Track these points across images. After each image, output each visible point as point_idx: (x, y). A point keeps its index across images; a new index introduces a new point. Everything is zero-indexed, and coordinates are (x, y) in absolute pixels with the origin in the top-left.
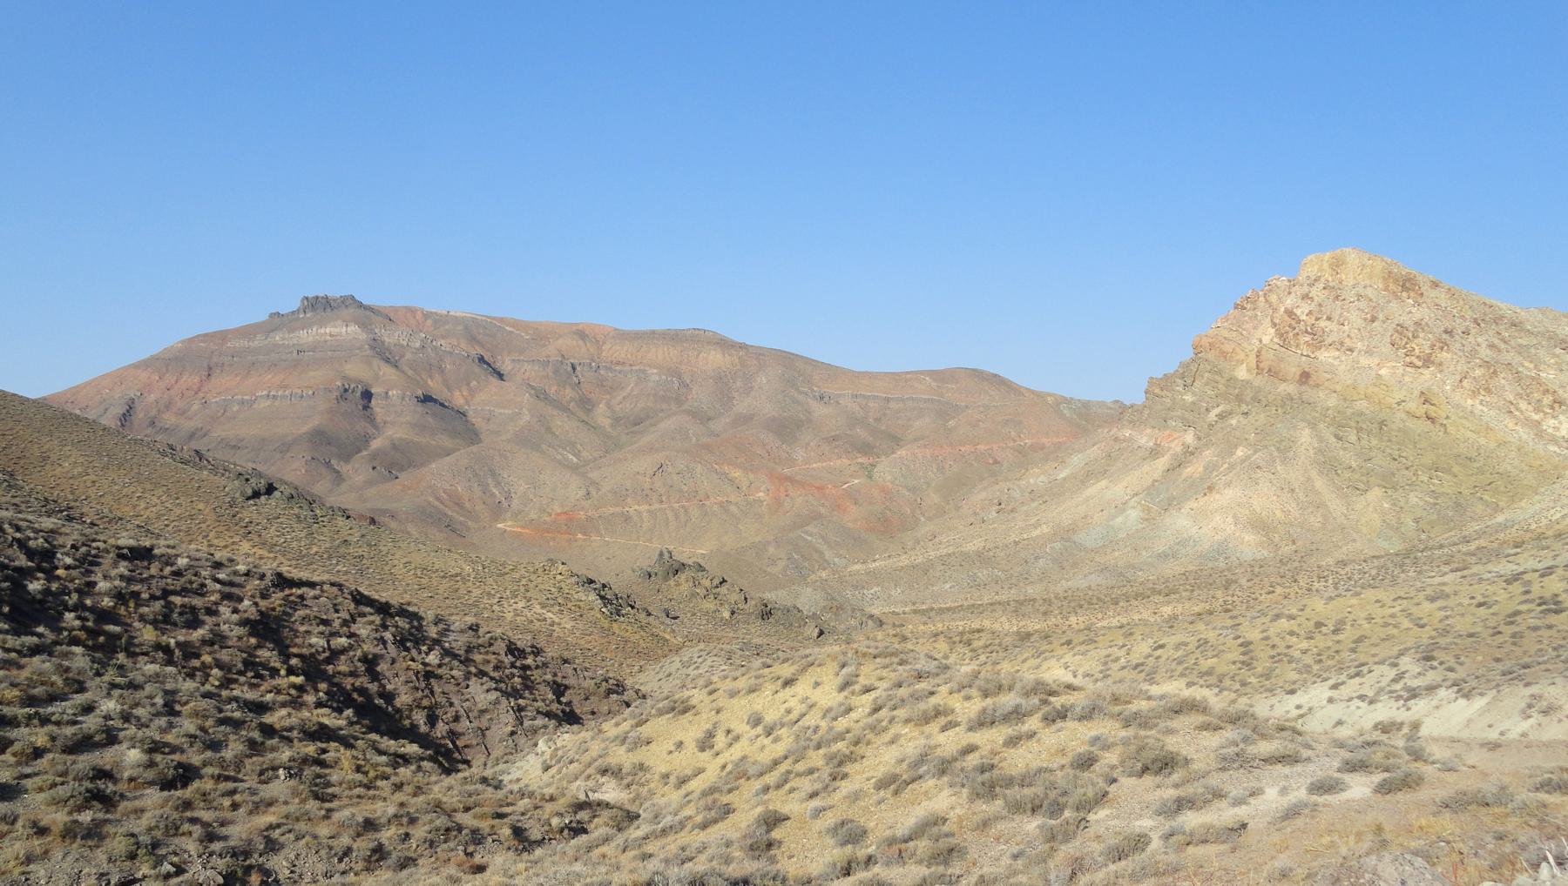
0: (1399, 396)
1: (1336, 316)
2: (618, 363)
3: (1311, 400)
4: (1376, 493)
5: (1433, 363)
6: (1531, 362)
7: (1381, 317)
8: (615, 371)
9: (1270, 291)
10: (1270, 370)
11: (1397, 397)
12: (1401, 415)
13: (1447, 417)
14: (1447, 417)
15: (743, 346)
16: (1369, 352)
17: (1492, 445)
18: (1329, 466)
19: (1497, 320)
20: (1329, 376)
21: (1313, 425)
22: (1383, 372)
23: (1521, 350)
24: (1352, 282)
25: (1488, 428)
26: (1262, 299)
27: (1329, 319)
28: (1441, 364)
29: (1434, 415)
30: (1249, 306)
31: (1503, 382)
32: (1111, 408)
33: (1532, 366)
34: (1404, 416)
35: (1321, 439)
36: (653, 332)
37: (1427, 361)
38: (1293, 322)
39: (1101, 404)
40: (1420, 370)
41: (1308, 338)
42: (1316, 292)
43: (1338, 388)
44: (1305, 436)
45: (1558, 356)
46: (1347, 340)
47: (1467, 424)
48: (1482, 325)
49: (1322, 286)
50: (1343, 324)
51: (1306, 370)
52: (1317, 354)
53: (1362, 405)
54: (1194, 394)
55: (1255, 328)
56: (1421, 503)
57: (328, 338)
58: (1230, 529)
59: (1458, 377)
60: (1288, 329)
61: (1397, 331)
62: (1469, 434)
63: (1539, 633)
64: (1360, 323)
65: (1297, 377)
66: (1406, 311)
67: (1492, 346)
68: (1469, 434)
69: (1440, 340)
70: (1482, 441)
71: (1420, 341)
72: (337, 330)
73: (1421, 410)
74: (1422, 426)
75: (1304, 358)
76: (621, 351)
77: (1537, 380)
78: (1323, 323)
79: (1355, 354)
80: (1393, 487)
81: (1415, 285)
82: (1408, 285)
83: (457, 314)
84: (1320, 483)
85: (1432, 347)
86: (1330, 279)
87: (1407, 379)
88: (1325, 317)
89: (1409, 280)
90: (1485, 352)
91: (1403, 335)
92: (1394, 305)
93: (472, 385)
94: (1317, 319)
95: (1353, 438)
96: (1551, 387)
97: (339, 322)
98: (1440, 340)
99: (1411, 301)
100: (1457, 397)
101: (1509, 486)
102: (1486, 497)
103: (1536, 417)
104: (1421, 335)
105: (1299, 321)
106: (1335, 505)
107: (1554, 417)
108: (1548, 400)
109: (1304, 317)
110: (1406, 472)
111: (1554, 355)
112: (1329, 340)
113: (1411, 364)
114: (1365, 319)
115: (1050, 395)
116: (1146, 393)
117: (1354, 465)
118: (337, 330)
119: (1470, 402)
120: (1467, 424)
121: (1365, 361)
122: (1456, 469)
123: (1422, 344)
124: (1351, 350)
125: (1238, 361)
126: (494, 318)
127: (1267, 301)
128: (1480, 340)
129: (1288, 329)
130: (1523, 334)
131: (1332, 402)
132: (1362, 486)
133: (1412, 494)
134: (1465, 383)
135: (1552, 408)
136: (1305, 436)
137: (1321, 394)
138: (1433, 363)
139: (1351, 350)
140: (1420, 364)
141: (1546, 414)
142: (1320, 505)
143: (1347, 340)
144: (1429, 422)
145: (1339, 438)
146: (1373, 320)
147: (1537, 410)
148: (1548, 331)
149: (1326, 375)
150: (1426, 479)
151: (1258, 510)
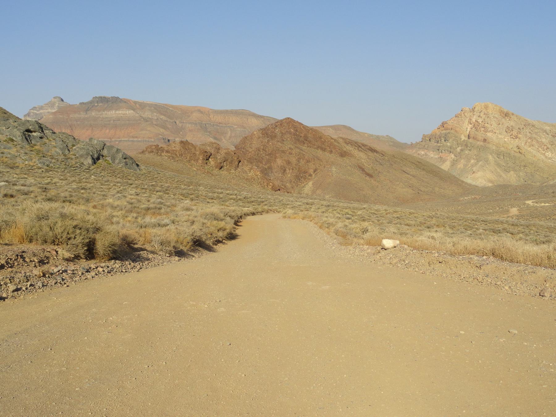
0: (511, 146)
1: (489, 123)
2: (220, 123)
3: (489, 147)
4: (512, 173)
5: (518, 138)
6: (539, 137)
7: (501, 123)
8: (220, 126)
9: (465, 112)
10: (473, 138)
11: (511, 147)
12: (513, 152)
13: (525, 153)
14: (525, 153)
15: (262, 117)
16: (500, 134)
17: (536, 160)
18: (499, 165)
19: (529, 124)
20: (492, 140)
21: (491, 154)
22: (506, 140)
23: (536, 133)
24: (491, 113)
25: (535, 156)
26: (463, 114)
27: (488, 123)
28: (520, 138)
29: (521, 152)
30: (460, 116)
31: (534, 143)
32: (386, 138)
33: (539, 138)
34: (514, 152)
35: (494, 158)
36: (227, 111)
37: (517, 137)
38: (478, 124)
39: (383, 137)
40: (515, 139)
41: (483, 129)
42: (482, 114)
43: (495, 144)
44: (490, 157)
45: (545, 135)
46: (494, 130)
47: (530, 155)
48: (526, 126)
49: (483, 113)
50: (492, 125)
51: (485, 138)
52: (487, 134)
53: (502, 149)
54: (450, 143)
55: (463, 123)
56: (523, 175)
57: (122, 115)
58: (485, 183)
59: (525, 142)
60: (476, 126)
61: (507, 129)
62: (531, 157)
63: (168, 227)
64: (496, 125)
65: (482, 140)
66: (507, 123)
67: (530, 133)
68: (531, 157)
69: (519, 132)
70: (534, 159)
71: (514, 132)
72: (124, 112)
73: (518, 151)
74: (518, 155)
75: (483, 135)
76: (218, 119)
77: (541, 142)
78: (486, 125)
79: (497, 134)
80: (515, 171)
81: (509, 115)
82: (507, 115)
83: (148, 103)
84: (498, 170)
85: (517, 133)
86: (485, 111)
87: (512, 142)
88: (486, 123)
89: (508, 113)
90: (528, 134)
91: (509, 130)
92: (503, 120)
93: (181, 133)
94: (485, 124)
95: (502, 158)
96: (545, 144)
97: (125, 109)
98: (519, 132)
99: (508, 119)
100: (526, 147)
101: (542, 171)
102: (537, 173)
103: (543, 152)
104: (514, 130)
105: (480, 124)
106: (504, 175)
107: (548, 152)
108: (545, 147)
109: (480, 123)
110: (517, 167)
111: (544, 135)
112: (489, 130)
113: (512, 138)
114: (497, 124)
115: (366, 133)
116: (422, 139)
117: (504, 165)
118: (124, 112)
119: (529, 149)
120: (530, 155)
121: (500, 136)
122: (530, 166)
123: (515, 133)
124: (495, 133)
125: (460, 133)
126: (163, 104)
127: (464, 115)
128: (527, 131)
129: (476, 126)
130: (536, 129)
131: (494, 148)
132: (508, 171)
133: (521, 172)
134: (527, 144)
135: (547, 150)
136: (490, 157)
137: (490, 145)
138: (518, 138)
139: (495, 133)
140: (515, 138)
141: (546, 151)
142: (501, 176)
143: (494, 130)
144: (520, 154)
145: (499, 158)
146: (499, 124)
147: (543, 150)
148: (541, 128)
149: (491, 140)
150: (523, 169)
151: (488, 177)
